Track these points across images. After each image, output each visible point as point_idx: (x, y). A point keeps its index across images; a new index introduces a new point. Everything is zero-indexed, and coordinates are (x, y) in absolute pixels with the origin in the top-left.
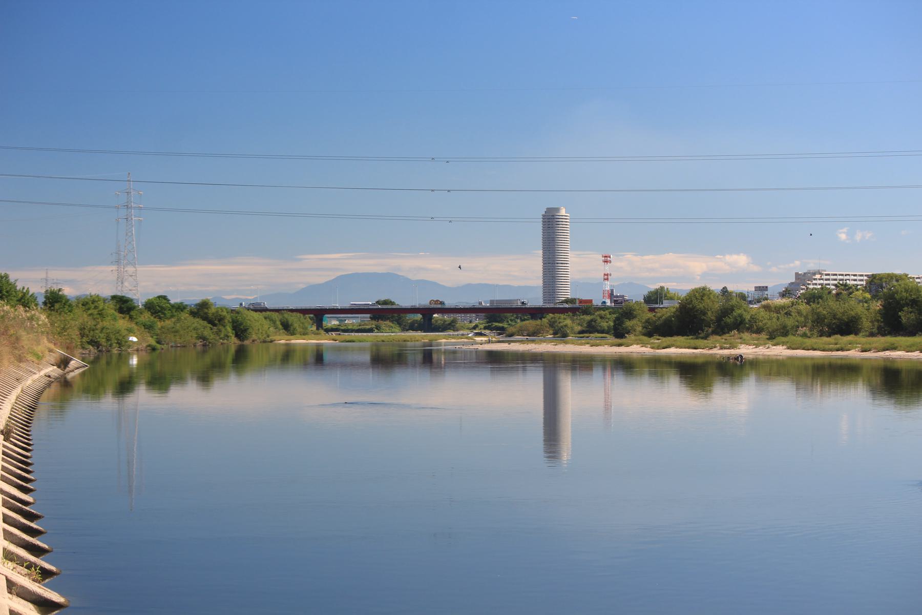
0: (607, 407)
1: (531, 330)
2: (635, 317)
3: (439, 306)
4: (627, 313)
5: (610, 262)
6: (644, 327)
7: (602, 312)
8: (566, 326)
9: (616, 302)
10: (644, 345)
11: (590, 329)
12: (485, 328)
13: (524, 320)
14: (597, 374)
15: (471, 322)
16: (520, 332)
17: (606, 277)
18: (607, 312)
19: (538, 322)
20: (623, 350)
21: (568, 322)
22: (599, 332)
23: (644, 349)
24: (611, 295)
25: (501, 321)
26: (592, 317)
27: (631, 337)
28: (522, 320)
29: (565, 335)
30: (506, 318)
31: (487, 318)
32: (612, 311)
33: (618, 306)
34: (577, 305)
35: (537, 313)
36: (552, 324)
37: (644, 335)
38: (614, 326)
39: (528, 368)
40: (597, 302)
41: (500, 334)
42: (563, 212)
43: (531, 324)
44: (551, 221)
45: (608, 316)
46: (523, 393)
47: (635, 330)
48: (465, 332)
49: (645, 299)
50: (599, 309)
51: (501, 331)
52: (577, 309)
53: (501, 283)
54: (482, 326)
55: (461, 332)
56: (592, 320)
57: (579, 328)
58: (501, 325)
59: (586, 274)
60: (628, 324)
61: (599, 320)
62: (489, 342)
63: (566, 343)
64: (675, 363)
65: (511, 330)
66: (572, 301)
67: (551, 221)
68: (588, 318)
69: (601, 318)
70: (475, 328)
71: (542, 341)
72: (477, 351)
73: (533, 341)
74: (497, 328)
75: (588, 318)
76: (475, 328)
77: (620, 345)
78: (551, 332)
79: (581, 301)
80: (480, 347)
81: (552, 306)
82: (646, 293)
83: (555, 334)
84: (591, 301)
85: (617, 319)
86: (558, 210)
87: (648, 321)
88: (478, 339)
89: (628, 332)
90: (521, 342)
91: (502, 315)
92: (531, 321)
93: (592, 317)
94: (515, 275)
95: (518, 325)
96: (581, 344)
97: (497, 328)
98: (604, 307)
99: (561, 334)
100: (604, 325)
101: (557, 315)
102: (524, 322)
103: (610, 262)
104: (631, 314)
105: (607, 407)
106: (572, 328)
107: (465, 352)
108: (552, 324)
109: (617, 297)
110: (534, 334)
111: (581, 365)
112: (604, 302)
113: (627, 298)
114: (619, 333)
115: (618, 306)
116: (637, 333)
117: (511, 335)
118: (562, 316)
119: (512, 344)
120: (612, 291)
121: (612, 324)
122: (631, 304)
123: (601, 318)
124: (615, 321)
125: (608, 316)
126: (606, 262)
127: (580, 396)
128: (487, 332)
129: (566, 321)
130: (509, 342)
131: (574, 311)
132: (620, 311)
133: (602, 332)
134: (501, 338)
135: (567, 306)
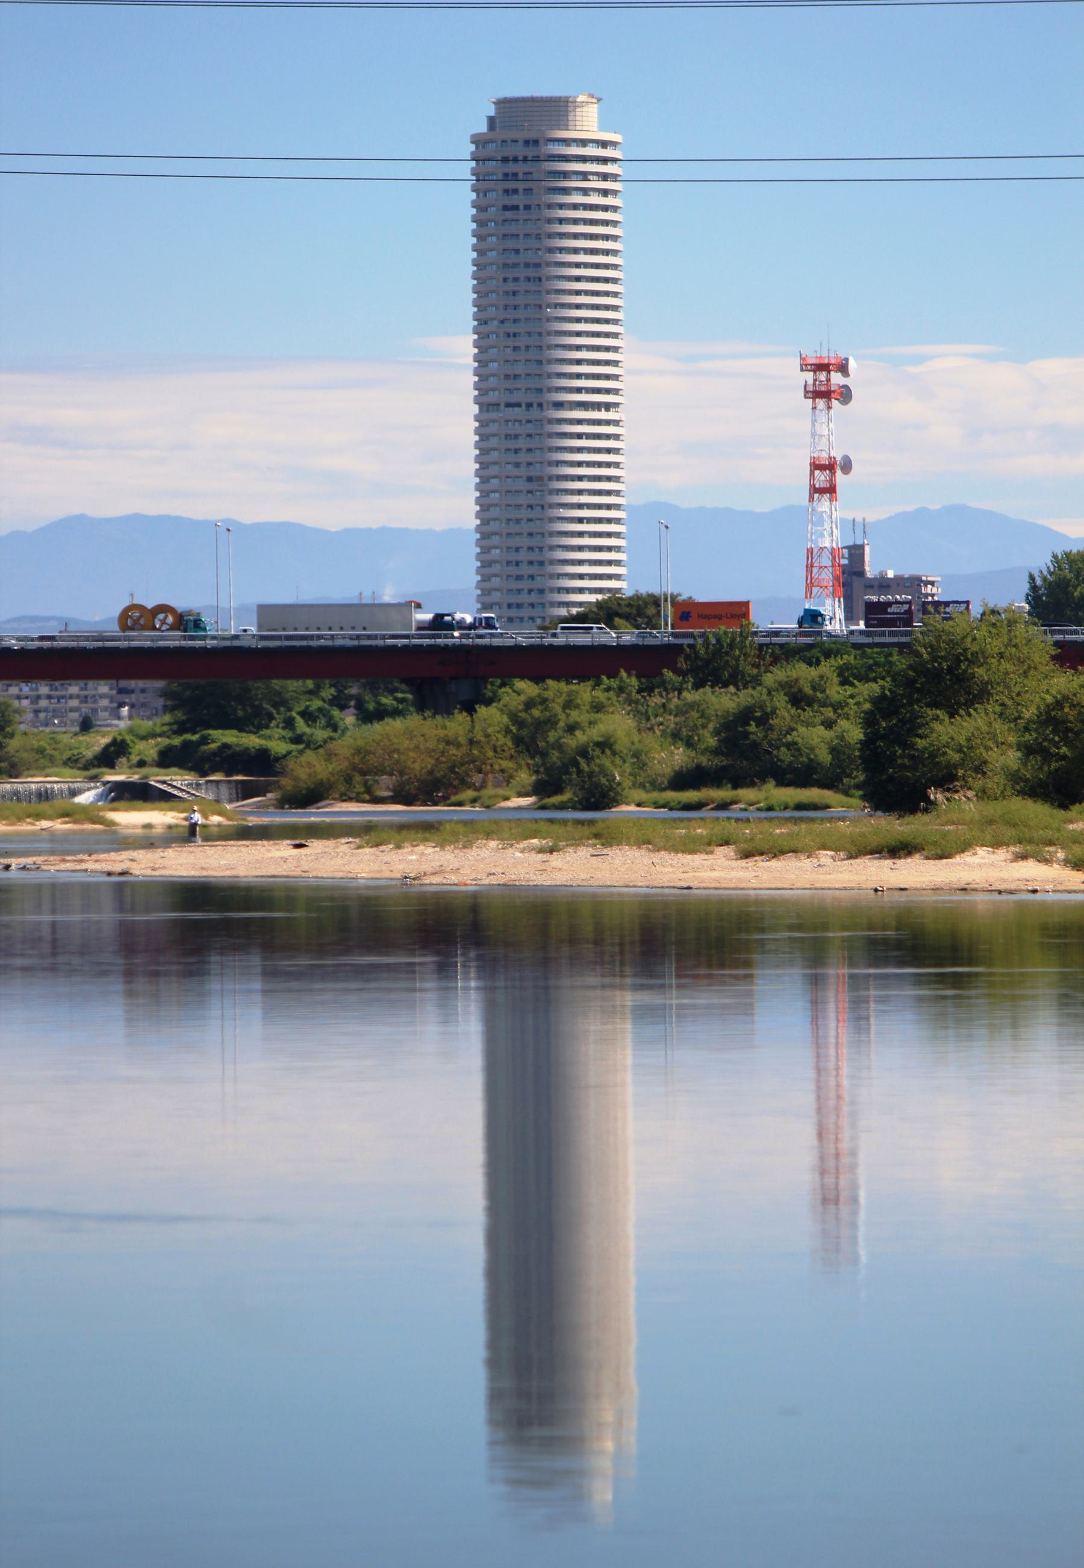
0: (833, 1196)
1: (419, 766)
2: (979, 695)
3: (174, 640)
4: (935, 676)
5: (845, 395)
6: (1028, 750)
7: (802, 673)
8: (605, 745)
9: (875, 613)
10: (1031, 847)
11: (739, 764)
12: (167, 759)
13: (380, 714)
14: (779, 1003)
15: (86, 725)
16: (359, 780)
17: (826, 475)
18: (828, 668)
19: (457, 724)
20: (915, 874)
21: (619, 723)
22: (787, 777)
23: (1031, 872)
24: (851, 573)
25: (255, 721)
26: (746, 697)
27: (957, 807)
28: (367, 717)
29: (599, 797)
30: (281, 702)
31: (174, 701)
32: (856, 661)
33: (887, 636)
34: (663, 634)
35: (437, 670)
36: (528, 736)
37: (1034, 791)
38: (867, 744)
39: (214, 968)
40: (775, 614)
41: (245, 792)
42: (588, 122)
43: (413, 735)
44: (523, 175)
45: (835, 691)
46: (390, 1107)
47: (980, 769)
48: (55, 781)
49: (1034, 597)
50: (779, 651)
51: (254, 772)
52: (666, 654)
53: (248, 515)
54: (149, 749)
55: (34, 782)
56: (745, 715)
57: (679, 757)
58: (251, 741)
59: (708, 472)
60: (945, 731)
61: (784, 712)
62: (191, 833)
63: (606, 838)
64: (1046, 929)
65: (308, 767)
66: (639, 610)
67: (523, 175)
68: (724, 701)
69: (798, 699)
70: (109, 757)
71: (469, 833)
72: (123, 889)
73: (427, 830)
74: (229, 761)
75: (724, 701)
76: (109, 757)
77: (898, 850)
78: (525, 778)
79: (688, 612)
80: (144, 865)
81: (522, 636)
82: (1040, 562)
83: (545, 788)
84: (738, 611)
85: (883, 706)
86: (557, 109)
87: (1051, 718)
88: (131, 818)
89: (947, 780)
90: (366, 833)
91: (258, 687)
92: (414, 721)
93: (746, 697)
94: (324, 461)
95: (344, 746)
96: (690, 846)
97: (229, 761)
98: (809, 643)
99: (576, 790)
100: (815, 738)
101: (555, 687)
102: (377, 728)
103: (845, 395)
104: (962, 680)
105: (833, 1196)
106: (638, 756)
107: (56, 893)
108: (528, 736)
109: (883, 584)
110: (432, 790)
111: (691, 950)
112: (813, 617)
113: (938, 593)
114: (897, 780)
115: (887, 636)
116: (995, 782)
117: (310, 796)
118: (585, 692)
119: (316, 846)
120: (856, 552)
121: (855, 733)
122: (958, 627)
123: (798, 699)
124: (869, 721)
125: (835, 691)
126: (821, 394)
127: (701, 1132)
128: (179, 780)
129: (608, 719)
130: (300, 835)
131: (649, 664)
132: (900, 662)
133: (804, 775)
134: (254, 812)
135: (609, 636)
